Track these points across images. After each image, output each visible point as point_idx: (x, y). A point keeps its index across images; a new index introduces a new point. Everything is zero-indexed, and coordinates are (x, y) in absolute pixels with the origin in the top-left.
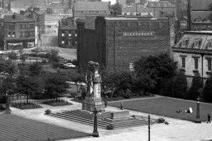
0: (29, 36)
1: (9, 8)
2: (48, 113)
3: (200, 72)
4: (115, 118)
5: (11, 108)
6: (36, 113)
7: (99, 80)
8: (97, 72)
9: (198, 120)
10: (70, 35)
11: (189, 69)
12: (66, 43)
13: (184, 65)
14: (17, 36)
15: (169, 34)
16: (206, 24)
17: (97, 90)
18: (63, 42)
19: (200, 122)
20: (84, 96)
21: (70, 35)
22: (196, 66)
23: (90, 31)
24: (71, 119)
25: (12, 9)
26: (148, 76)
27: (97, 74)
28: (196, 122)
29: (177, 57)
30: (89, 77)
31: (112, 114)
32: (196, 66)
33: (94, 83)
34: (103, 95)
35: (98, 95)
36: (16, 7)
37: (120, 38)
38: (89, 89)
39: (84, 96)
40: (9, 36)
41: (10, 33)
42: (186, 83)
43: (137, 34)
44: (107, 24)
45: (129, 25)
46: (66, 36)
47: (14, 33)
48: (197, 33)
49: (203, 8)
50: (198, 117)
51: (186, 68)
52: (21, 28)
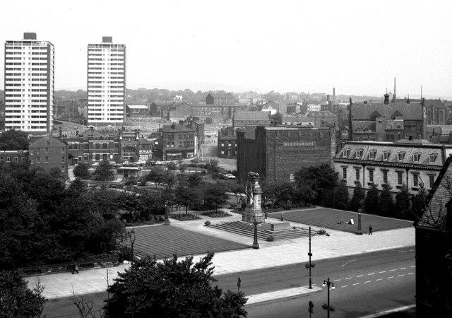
0: (188, 146)
1: (168, 118)
2: (207, 224)
3: (362, 182)
4: (275, 229)
7: (260, 191)
8: (257, 183)
9: (359, 232)
10: (230, 145)
12: (226, 154)
14: (177, 146)
15: (330, 144)
17: (257, 201)
18: (223, 153)
19: (361, 234)
20: (244, 207)
21: (230, 145)
23: (250, 141)
24: (231, 231)
27: (257, 185)
28: (357, 234)
29: (338, 168)
30: (249, 188)
31: (273, 226)
33: (255, 194)
34: (263, 206)
35: (258, 206)
36: (175, 116)
37: (280, 148)
38: (249, 200)
39: (244, 207)
40: (168, 146)
42: (347, 194)
44: (268, 135)
45: (289, 134)
47: (173, 143)
49: (365, 118)
50: (359, 228)
51: (347, 179)
52: (181, 138)
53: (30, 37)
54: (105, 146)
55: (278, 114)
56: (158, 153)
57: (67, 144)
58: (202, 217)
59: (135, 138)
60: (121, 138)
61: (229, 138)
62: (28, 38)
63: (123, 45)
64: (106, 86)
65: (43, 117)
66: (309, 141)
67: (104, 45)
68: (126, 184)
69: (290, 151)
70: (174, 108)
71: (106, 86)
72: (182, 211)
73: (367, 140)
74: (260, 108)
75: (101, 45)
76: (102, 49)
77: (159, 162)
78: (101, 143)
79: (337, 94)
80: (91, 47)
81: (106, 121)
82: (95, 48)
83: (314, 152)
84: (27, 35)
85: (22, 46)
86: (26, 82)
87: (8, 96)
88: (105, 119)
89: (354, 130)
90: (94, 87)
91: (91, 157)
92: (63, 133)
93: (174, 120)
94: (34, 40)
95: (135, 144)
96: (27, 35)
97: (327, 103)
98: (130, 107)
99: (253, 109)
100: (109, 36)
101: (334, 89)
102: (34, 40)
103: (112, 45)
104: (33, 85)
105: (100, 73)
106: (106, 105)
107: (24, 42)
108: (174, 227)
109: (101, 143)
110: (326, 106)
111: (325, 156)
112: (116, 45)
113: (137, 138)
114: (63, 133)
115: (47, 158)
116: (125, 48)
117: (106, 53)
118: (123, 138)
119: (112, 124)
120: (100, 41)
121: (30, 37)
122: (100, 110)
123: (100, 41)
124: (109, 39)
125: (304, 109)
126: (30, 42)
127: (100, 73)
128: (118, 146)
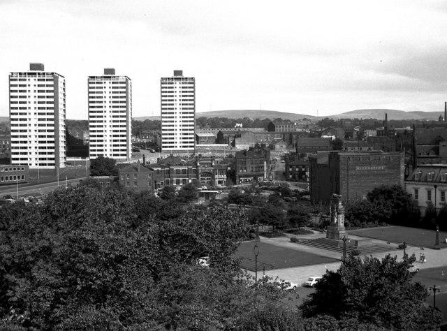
0: (259, 171)
1: (233, 144)
2: (293, 241)
3: (433, 202)
4: (359, 245)
5: (261, 237)
6: (281, 241)
7: (343, 211)
8: (340, 204)
9: (437, 247)
10: (297, 170)
11: (422, 200)
12: (294, 177)
13: (417, 197)
14: (248, 171)
15: (399, 168)
16: (431, 158)
17: (340, 220)
18: (291, 176)
19: (439, 249)
20: (325, 225)
21: (297, 170)
22: (429, 198)
23: (324, 166)
24: (315, 246)
25: (237, 146)
26: (154, 227)
27: (340, 206)
28: (434, 249)
29: (410, 189)
30: (333, 209)
31: (357, 242)
32: (429, 198)
33: (338, 214)
34: (346, 225)
35: (342, 225)
36: (241, 143)
37: (353, 172)
38: (333, 219)
39: (325, 225)
40: (241, 171)
41: (242, 169)
42: (420, 213)
43: (369, 168)
44: (341, 159)
45: (361, 160)
46: (294, 170)
47: (246, 168)
48: (428, 167)
49: (428, 142)
50: (437, 244)
51: (419, 200)
52: (252, 164)
53: (109, 73)
54: (184, 171)
55: (337, 139)
56: (232, 176)
57: (153, 170)
58: (287, 234)
59: (211, 164)
60: (198, 164)
61: (297, 163)
62: (109, 74)
63: (192, 78)
64: (108, 116)
65: (51, 148)
66: (379, 165)
67: (175, 79)
68: (209, 206)
69: (362, 175)
70: (240, 136)
71: (108, 116)
72: (266, 228)
73: (438, 163)
74: (320, 134)
75: (172, 78)
76: (27, 78)
77: (236, 186)
78: (181, 168)
79: (389, 119)
80: (164, 80)
81: (178, 149)
82: (168, 82)
83: (385, 175)
84: (107, 71)
85: (103, 81)
86: (108, 114)
87: (13, 125)
88: (178, 146)
89: (417, 153)
90: (167, 117)
91: (172, 181)
92: (147, 160)
93: (240, 147)
94: (113, 75)
95: (211, 170)
96: (33, 66)
97: (384, 128)
98: (199, 135)
99: (312, 135)
100: (179, 69)
101: (386, 115)
102: (113, 75)
103: (183, 78)
104: (39, 120)
105: (173, 105)
106: (178, 134)
107: (105, 77)
108: (264, 243)
109: (181, 168)
110: (382, 131)
111: (394, 179)
112: (186, 78)
113: (213, 164)
114: (147, 160)
115: (135, 183)
116: (194, 80)
117: (178, 85)
118: (201, 164)
119: (185, 152)
120: (172, 75)
121: (109, 73)
122: (25, 142)
123: (102, 74)
124: (40, 67)
125: (360, 135)
126: (110, 77)
127: (173, 105)
128: (196, 172)
